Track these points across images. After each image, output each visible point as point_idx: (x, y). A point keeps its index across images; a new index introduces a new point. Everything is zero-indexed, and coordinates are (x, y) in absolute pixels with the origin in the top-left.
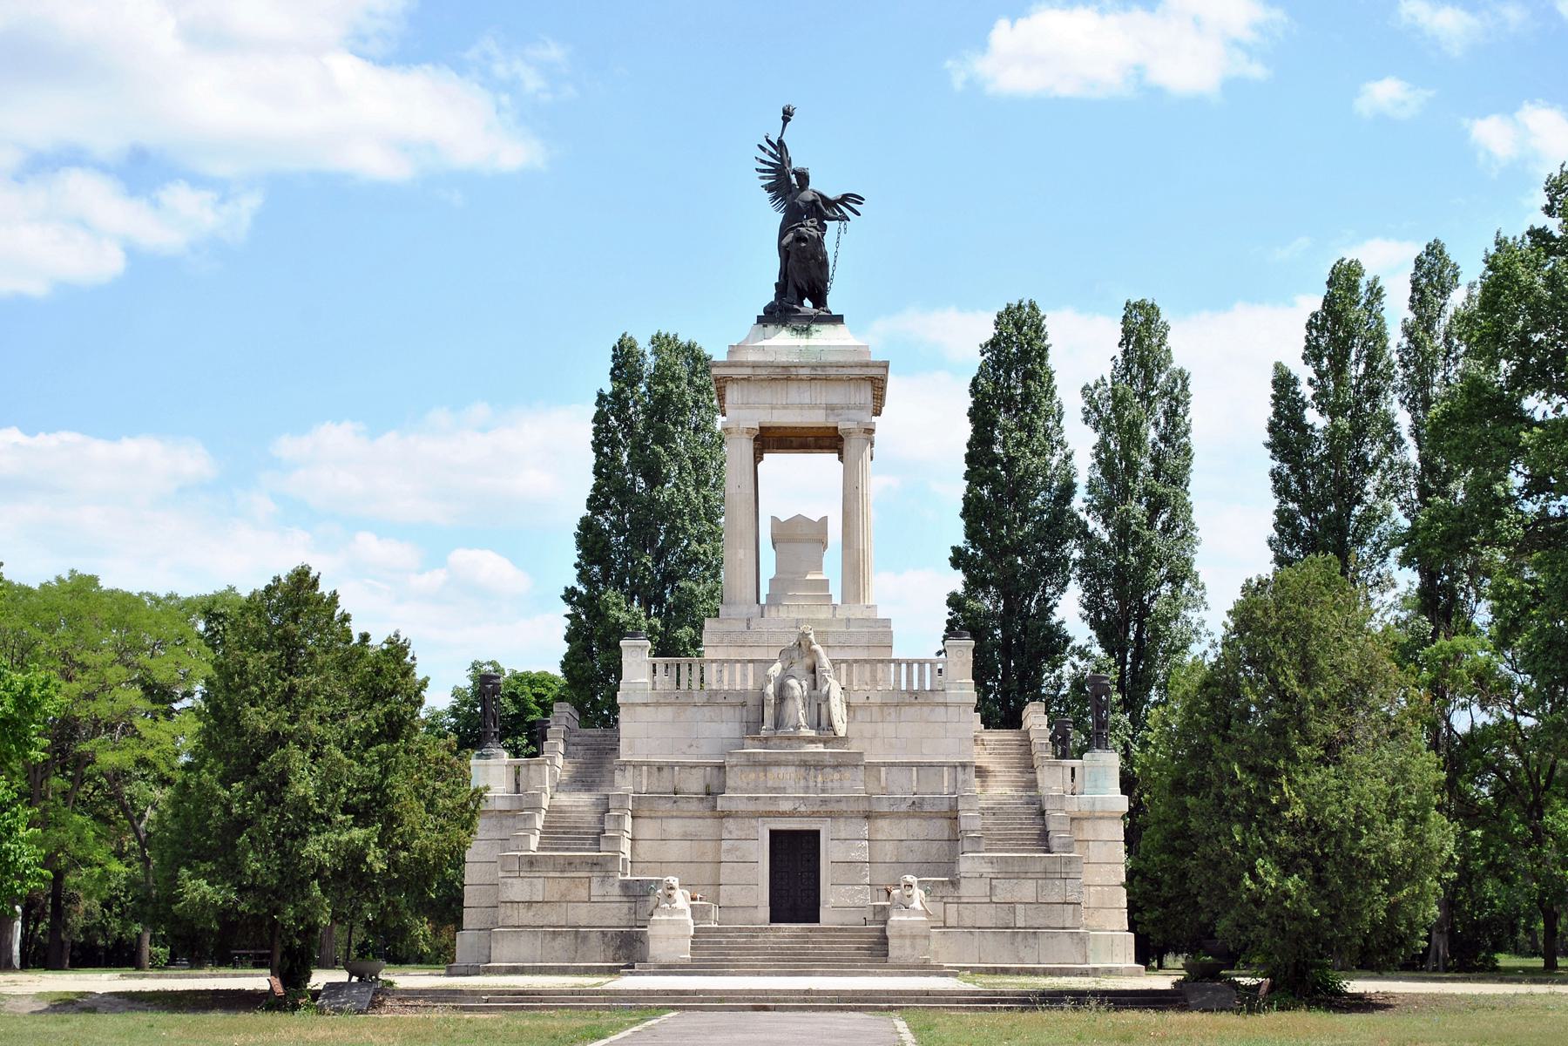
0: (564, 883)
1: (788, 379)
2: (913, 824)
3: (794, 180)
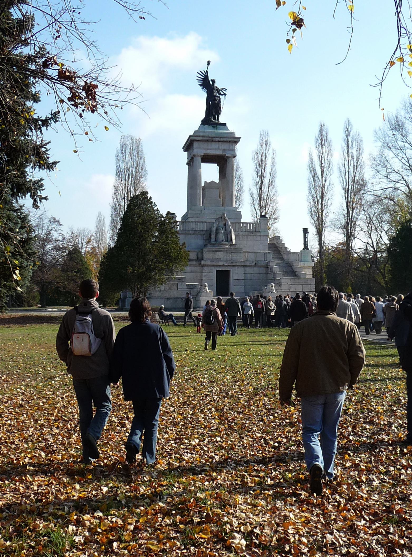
0: (170, 284)
1: (212, 141)
2: (256, 269)
3: (211, 83)
